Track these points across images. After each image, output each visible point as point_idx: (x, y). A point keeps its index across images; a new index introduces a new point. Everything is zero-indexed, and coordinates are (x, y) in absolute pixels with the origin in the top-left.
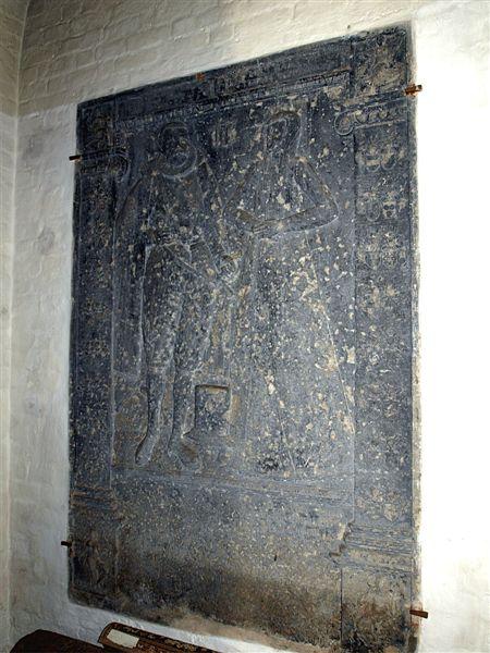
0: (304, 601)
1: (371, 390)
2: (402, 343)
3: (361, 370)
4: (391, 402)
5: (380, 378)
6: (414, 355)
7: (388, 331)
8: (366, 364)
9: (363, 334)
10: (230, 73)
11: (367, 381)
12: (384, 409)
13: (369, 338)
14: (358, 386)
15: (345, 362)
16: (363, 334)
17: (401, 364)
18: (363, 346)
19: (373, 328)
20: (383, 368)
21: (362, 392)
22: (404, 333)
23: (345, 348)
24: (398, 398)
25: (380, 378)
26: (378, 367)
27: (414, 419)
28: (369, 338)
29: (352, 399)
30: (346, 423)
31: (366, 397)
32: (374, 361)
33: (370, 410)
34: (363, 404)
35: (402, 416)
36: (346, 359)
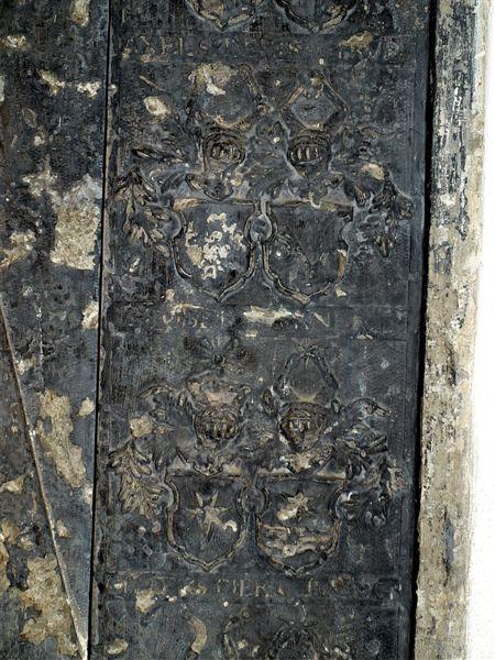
0: (471, 45)
1: (194, 420)
2: (375, 169)
3: (133, 311)
4: (302, 479)
5: (248, 357)
6: (441, 234)
7: (297, 97)
8: (163, 272)
9: (157, 107)
10: (415, 65)
11: (167, 364)
12: (257, 516)
13: (194, 131)
14: (111, 391)
15: (39, 263)
16: (157, 107)
17: (361, 278)
18: (153, 173)
19: (212, 80)
20: (263, 301)
21: (140, 425)
22: (386, 114)
23: (41, 182)
24: (336, 460)
25: (248, 357)
26: (234, 289)
27: (429, 572)
28: (194, 131)
29: (72, 465)
30: (35, 592)
31: (160, 455)
32: (211, 256)
33: (180, 527)
34: (141, 491)
35: (358, 553)
36: (47, 242)
